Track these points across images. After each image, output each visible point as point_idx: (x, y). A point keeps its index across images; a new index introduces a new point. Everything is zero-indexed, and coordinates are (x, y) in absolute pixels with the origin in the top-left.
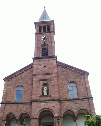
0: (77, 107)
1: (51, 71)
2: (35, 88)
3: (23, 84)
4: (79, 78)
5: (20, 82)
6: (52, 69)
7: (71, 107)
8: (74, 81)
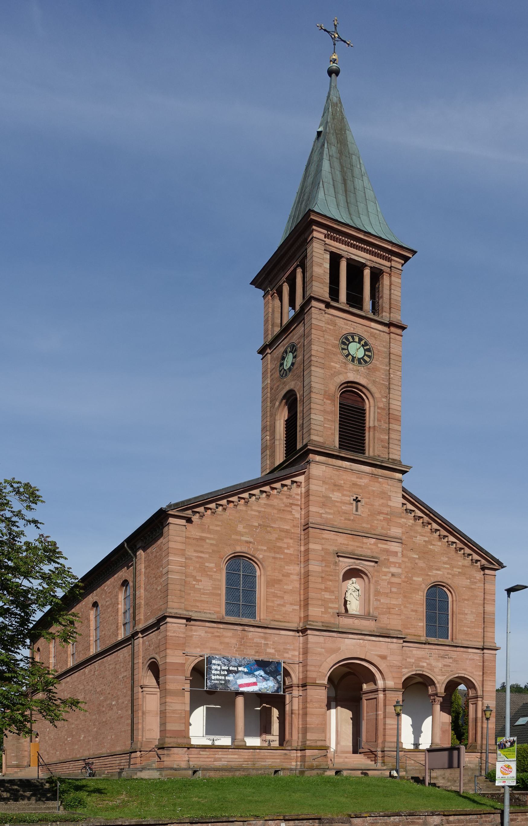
0: (449, 669)
1: (379, 526)
2: (320, 580)
3: (257, 550)
4: (465, 574)
5: (244, 538)
6: (385, 519)
7: (428, 664)
8: (449, 582)
